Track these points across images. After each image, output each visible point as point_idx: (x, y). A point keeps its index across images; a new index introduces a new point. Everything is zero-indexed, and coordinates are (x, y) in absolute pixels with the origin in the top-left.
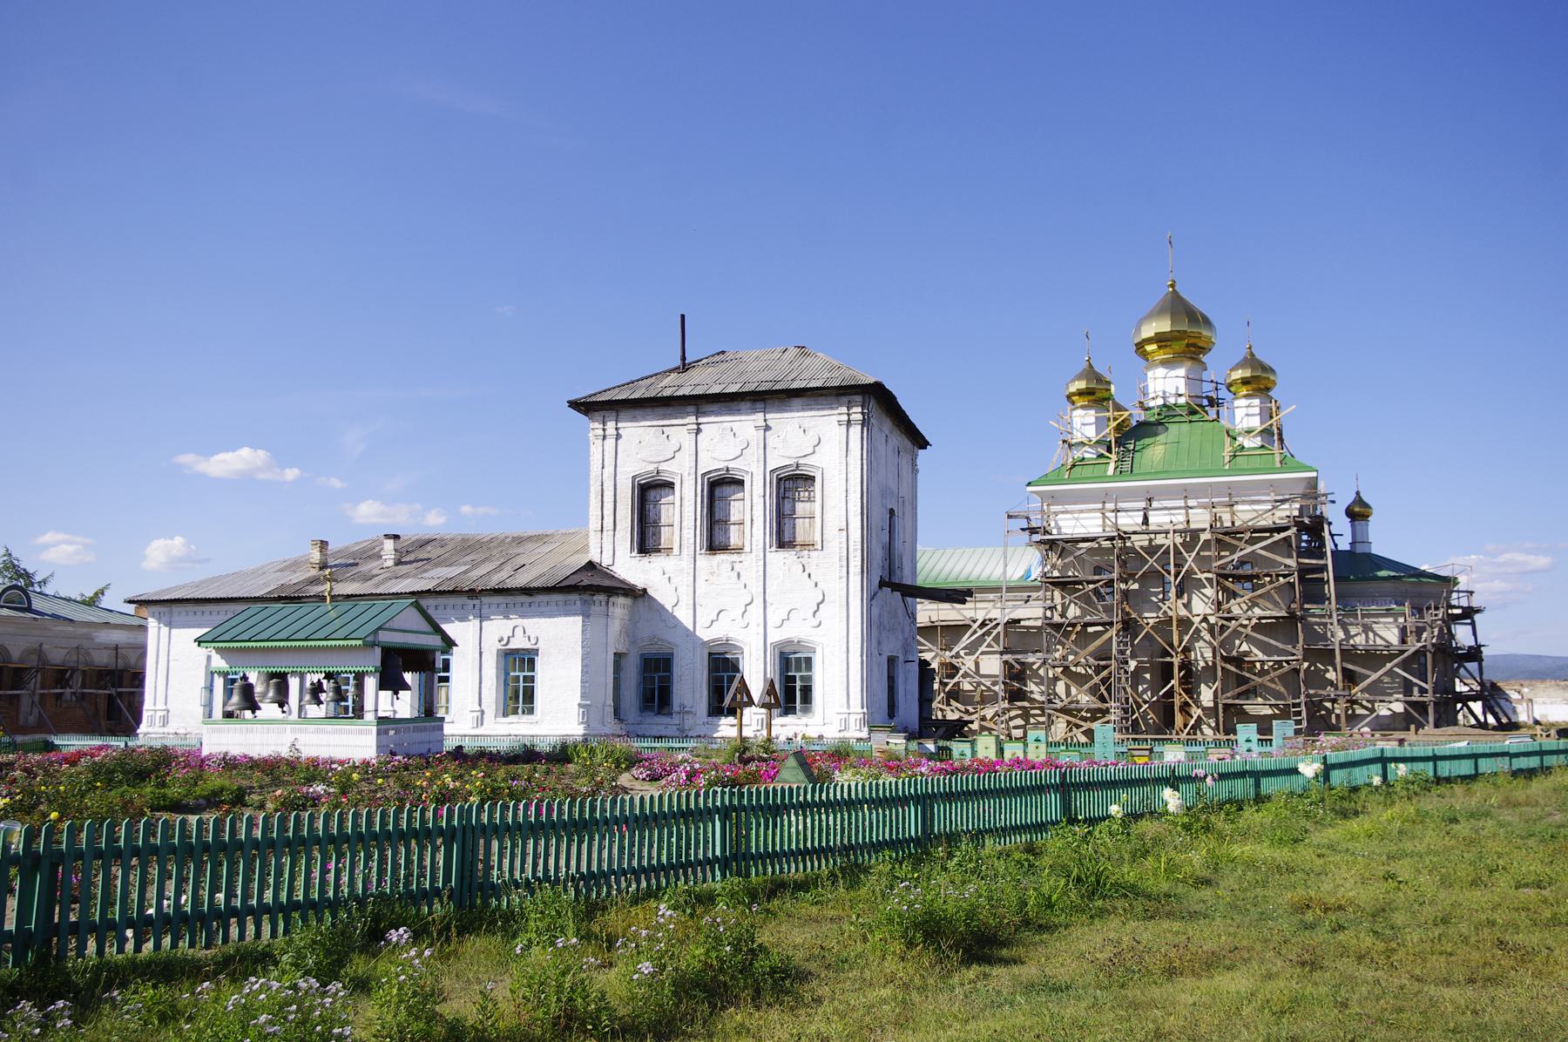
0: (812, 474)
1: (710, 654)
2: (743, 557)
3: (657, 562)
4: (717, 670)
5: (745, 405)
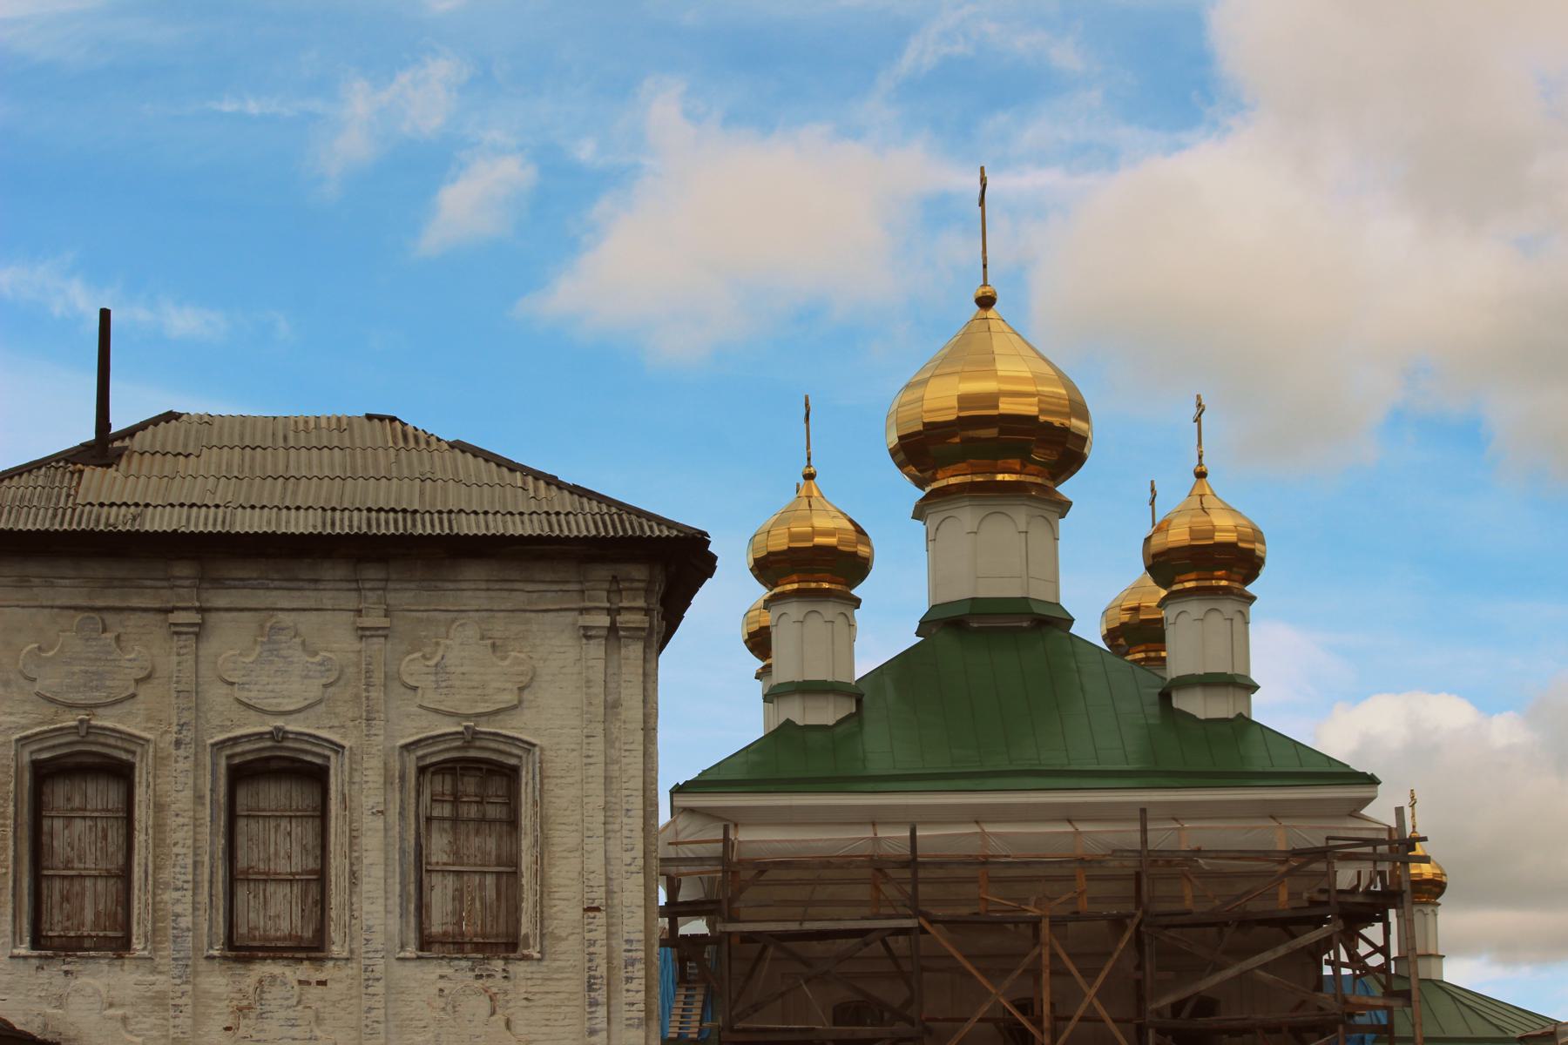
0: (513, 761)
2: (328, 971)
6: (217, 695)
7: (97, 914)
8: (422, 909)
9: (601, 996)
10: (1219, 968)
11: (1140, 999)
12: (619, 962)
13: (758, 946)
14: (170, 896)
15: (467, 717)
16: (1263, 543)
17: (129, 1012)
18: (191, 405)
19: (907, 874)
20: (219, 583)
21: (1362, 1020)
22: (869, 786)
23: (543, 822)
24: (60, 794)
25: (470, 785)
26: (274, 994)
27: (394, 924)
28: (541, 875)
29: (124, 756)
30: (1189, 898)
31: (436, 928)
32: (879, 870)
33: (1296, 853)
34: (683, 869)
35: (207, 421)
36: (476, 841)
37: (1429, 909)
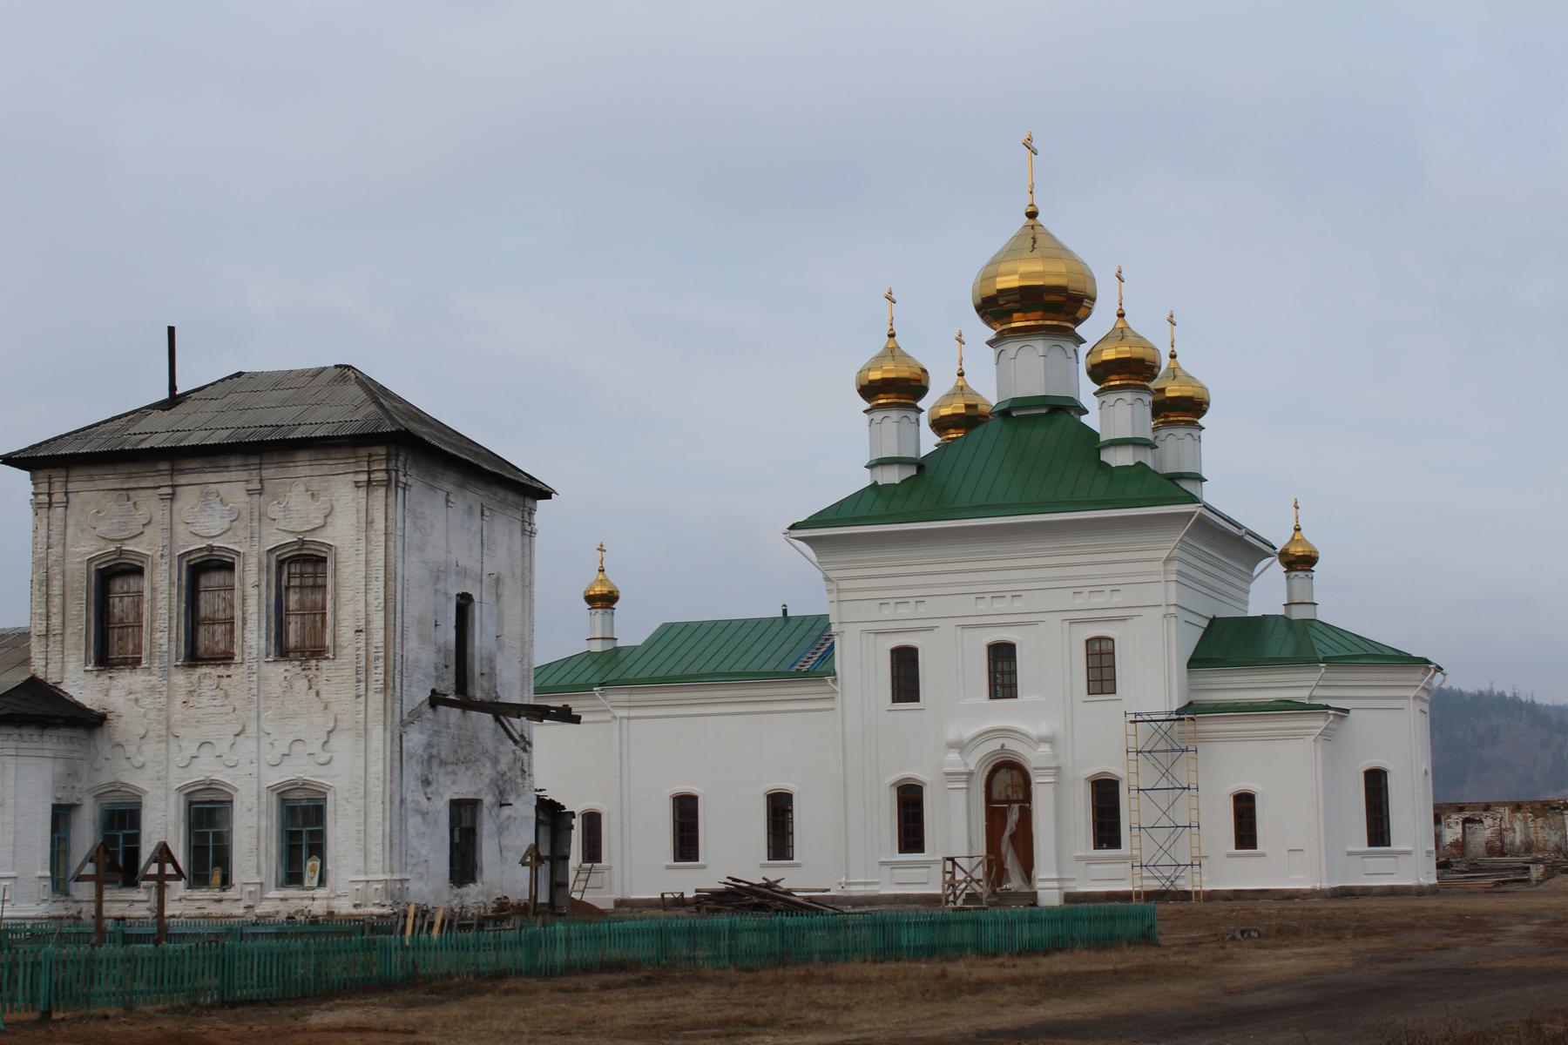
0: (324, 555)
3: (126, 680)
4: (200, 825)
5: (235, 461)
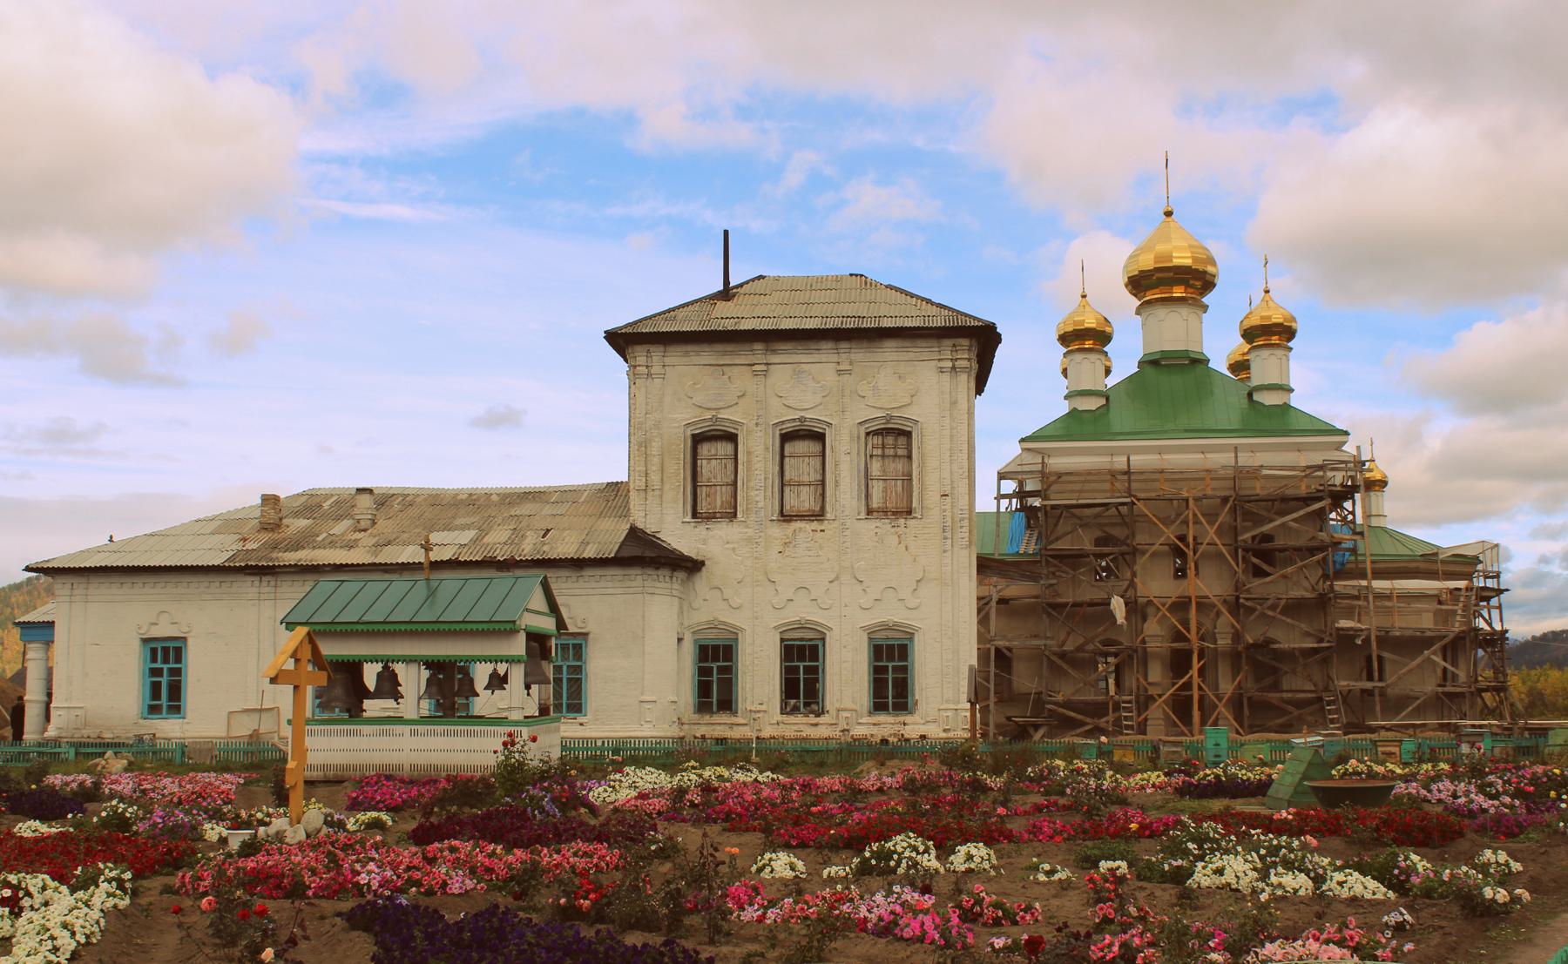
0: (909, 429)
1: (782, 640)
2: (825, 525)
6: (775, 403)
7: (722, 502)
8: (867, 496)
9: (948, 534)
10: (1272, 521)
11: (1236, 535)
12: (957, 519)
13: (1059, 511)
14: (753, 493)
15: (888, 409)
16: (1296, 322)
17: (735, 545)
18: (770, 272)
19: (1126, 477)
20: (774, 352)
21: (1343, 545)
22: (1121, 437)
23: (922, 456)
24: (705, 449)
25: (890, 440)
26: (801, 537)
27: (855, 503)
28: (921, 480)
29: (733, 431)
30: (1259, 489)
31: (875, 505)
32: (1113, 476)
33: (1308, 467)
34: (1025, 477)
35: (777, 279)
36: (893, 465)
37: (1379, 494)
